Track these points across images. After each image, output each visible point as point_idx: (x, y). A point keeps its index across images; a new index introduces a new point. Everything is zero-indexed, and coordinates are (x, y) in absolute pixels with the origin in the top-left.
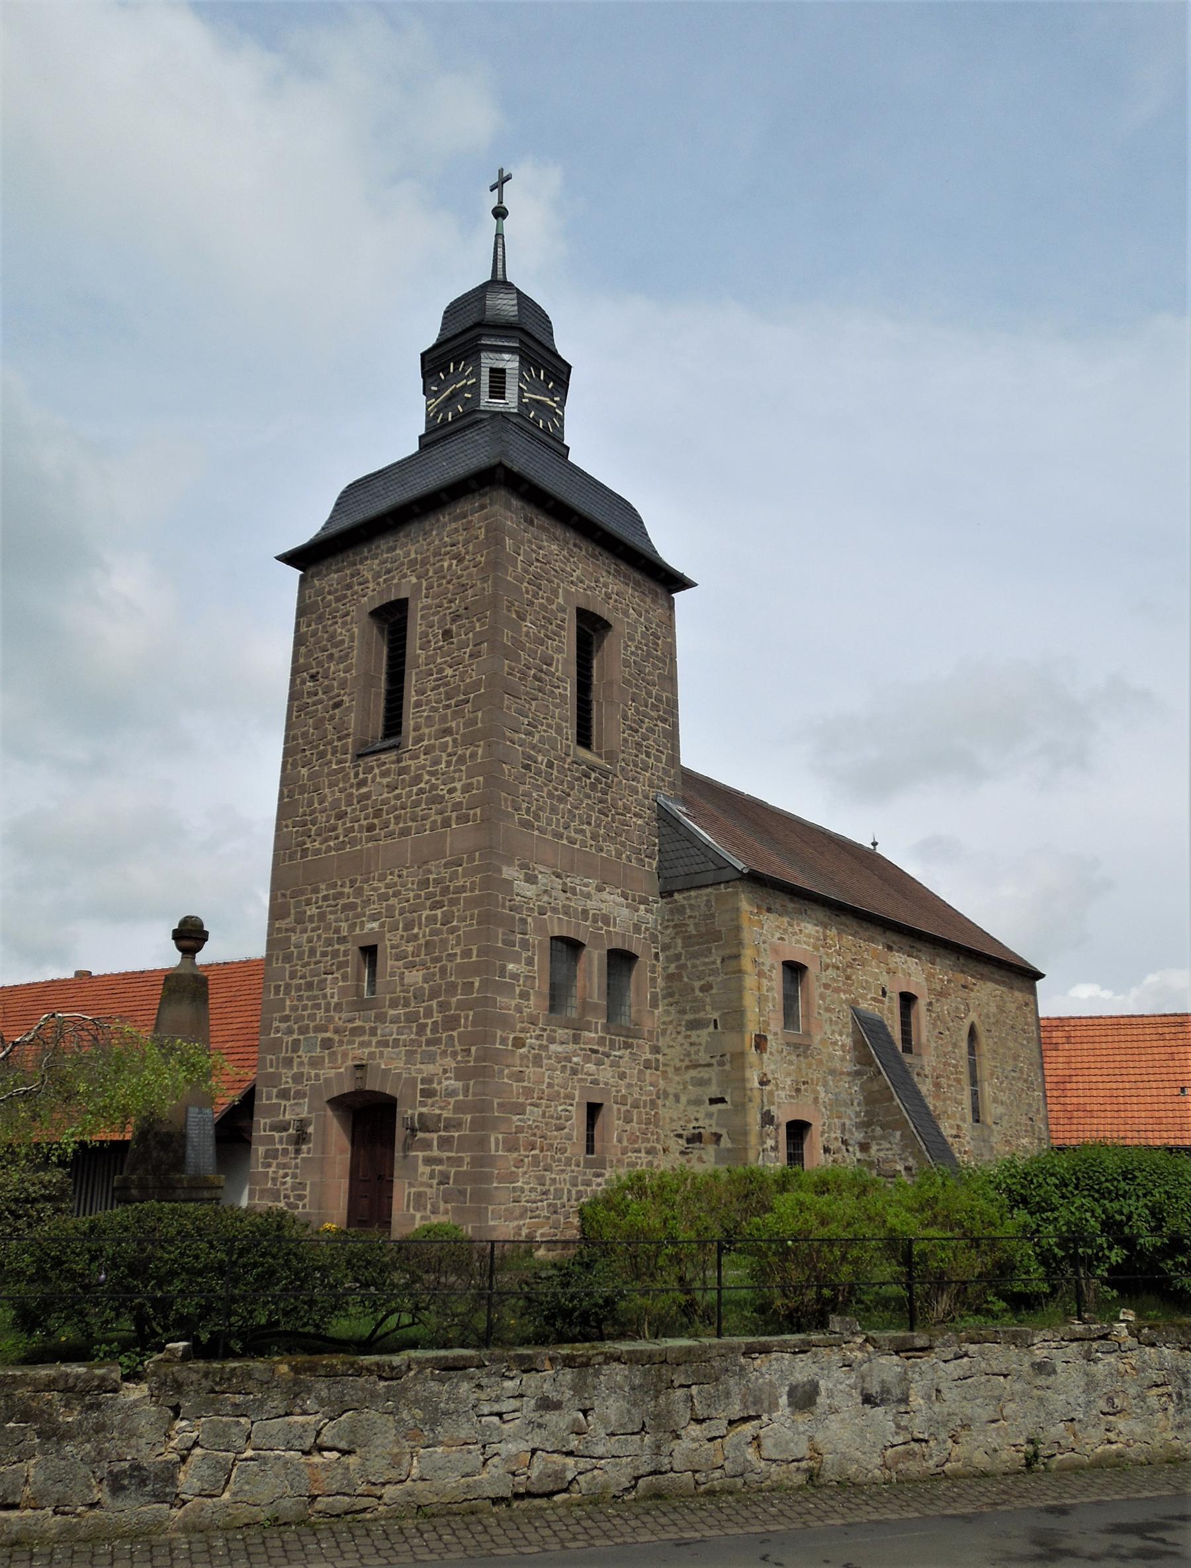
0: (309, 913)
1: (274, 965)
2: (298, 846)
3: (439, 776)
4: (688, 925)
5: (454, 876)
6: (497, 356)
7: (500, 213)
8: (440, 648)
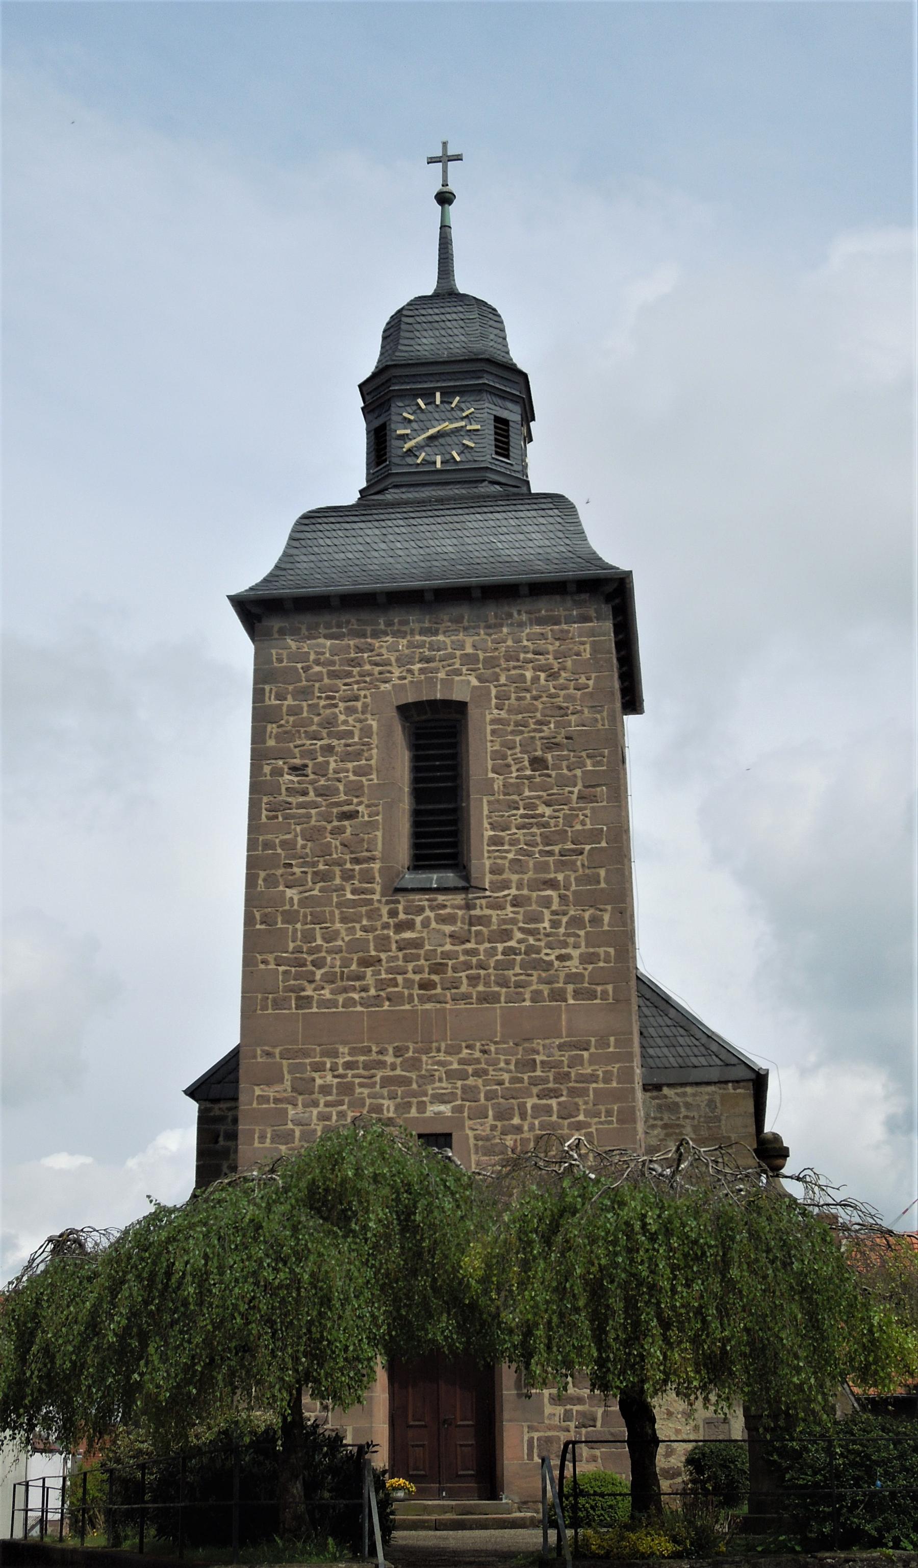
0: (319, 1082)
1: (256, 1145)
2: (292, 991)
3: (542, 937)
4: (683, 1126)
5: (576, 1062)
6: (500, 402)
7: (444, 199)
8: (529, 778)
